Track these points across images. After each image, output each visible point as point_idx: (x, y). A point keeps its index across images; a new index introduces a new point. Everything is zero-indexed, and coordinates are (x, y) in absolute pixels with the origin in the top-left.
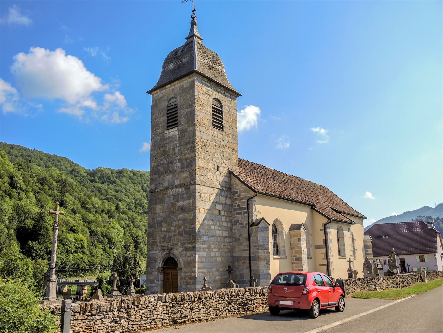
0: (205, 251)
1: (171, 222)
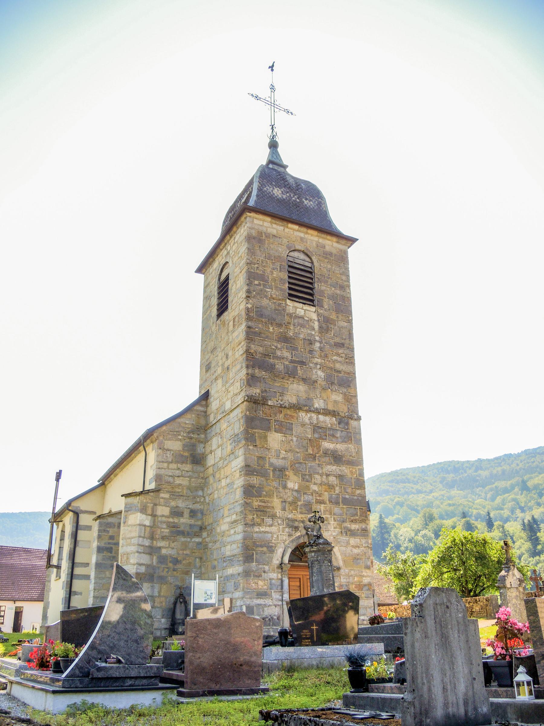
1: (310, 475)
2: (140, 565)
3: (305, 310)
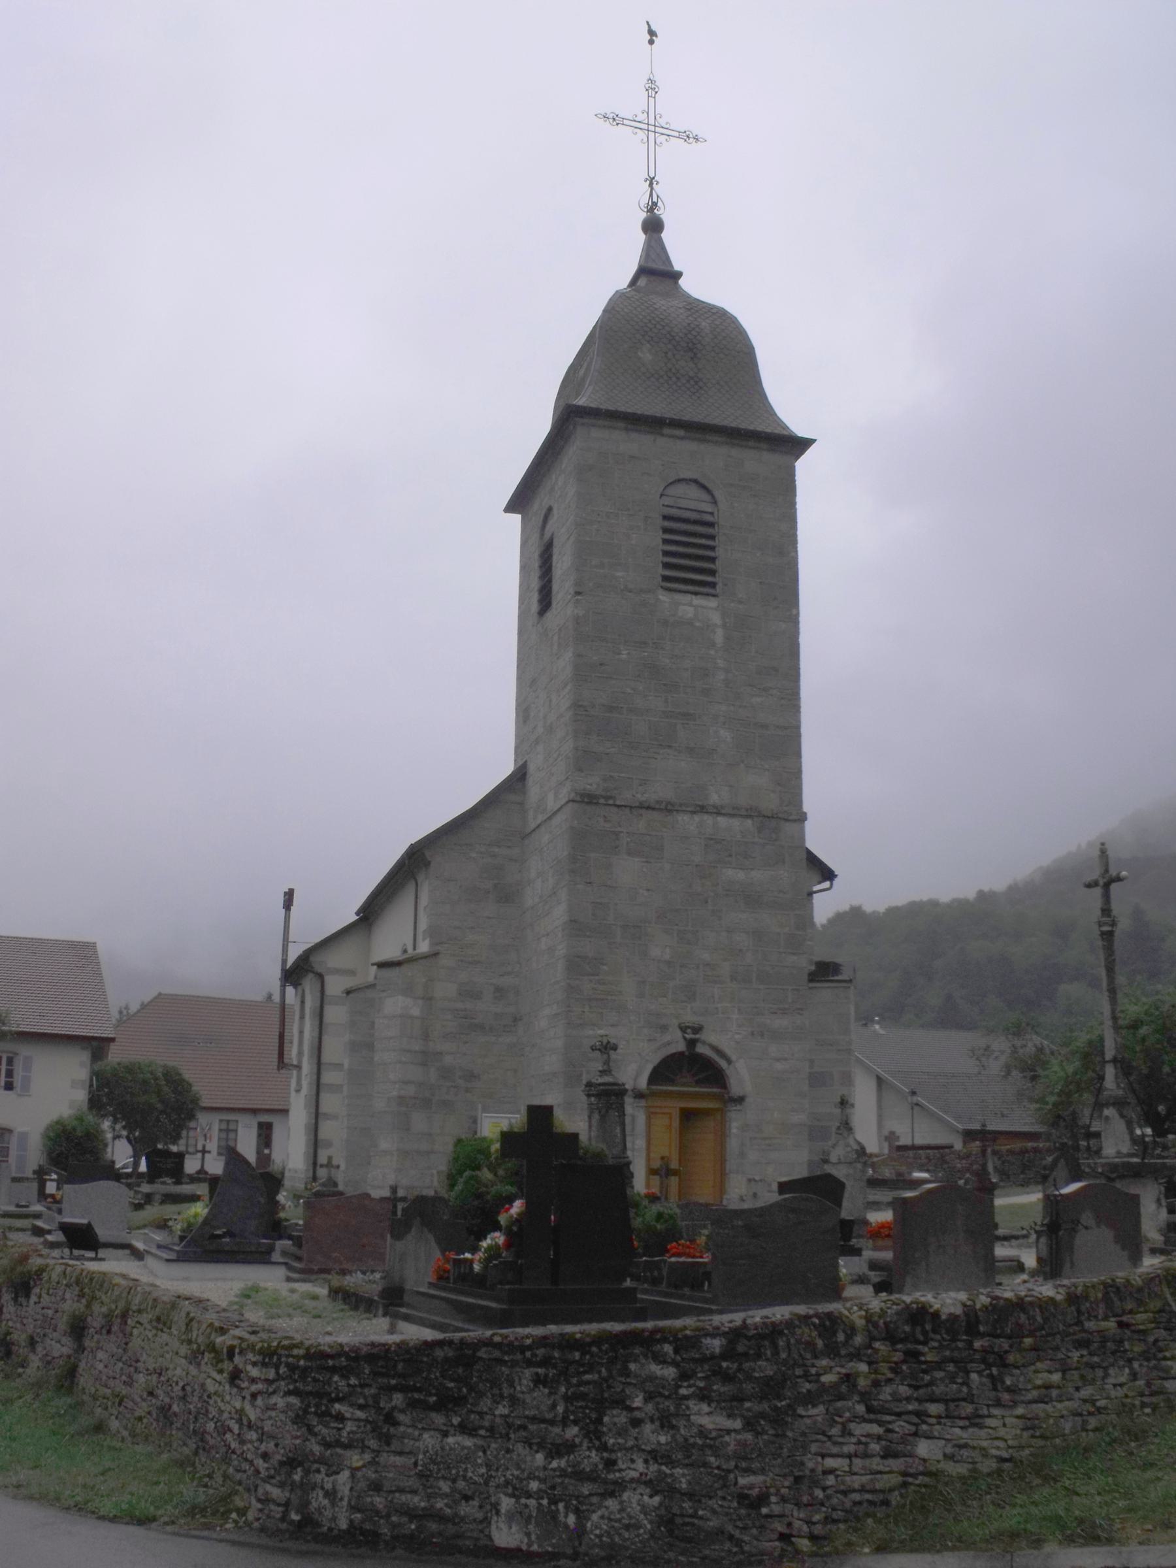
2: (406, 1083)
3: (696, 607)
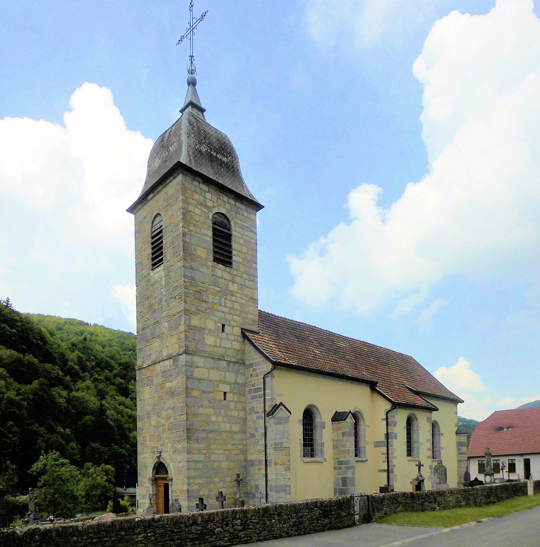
0: (202, 453)
